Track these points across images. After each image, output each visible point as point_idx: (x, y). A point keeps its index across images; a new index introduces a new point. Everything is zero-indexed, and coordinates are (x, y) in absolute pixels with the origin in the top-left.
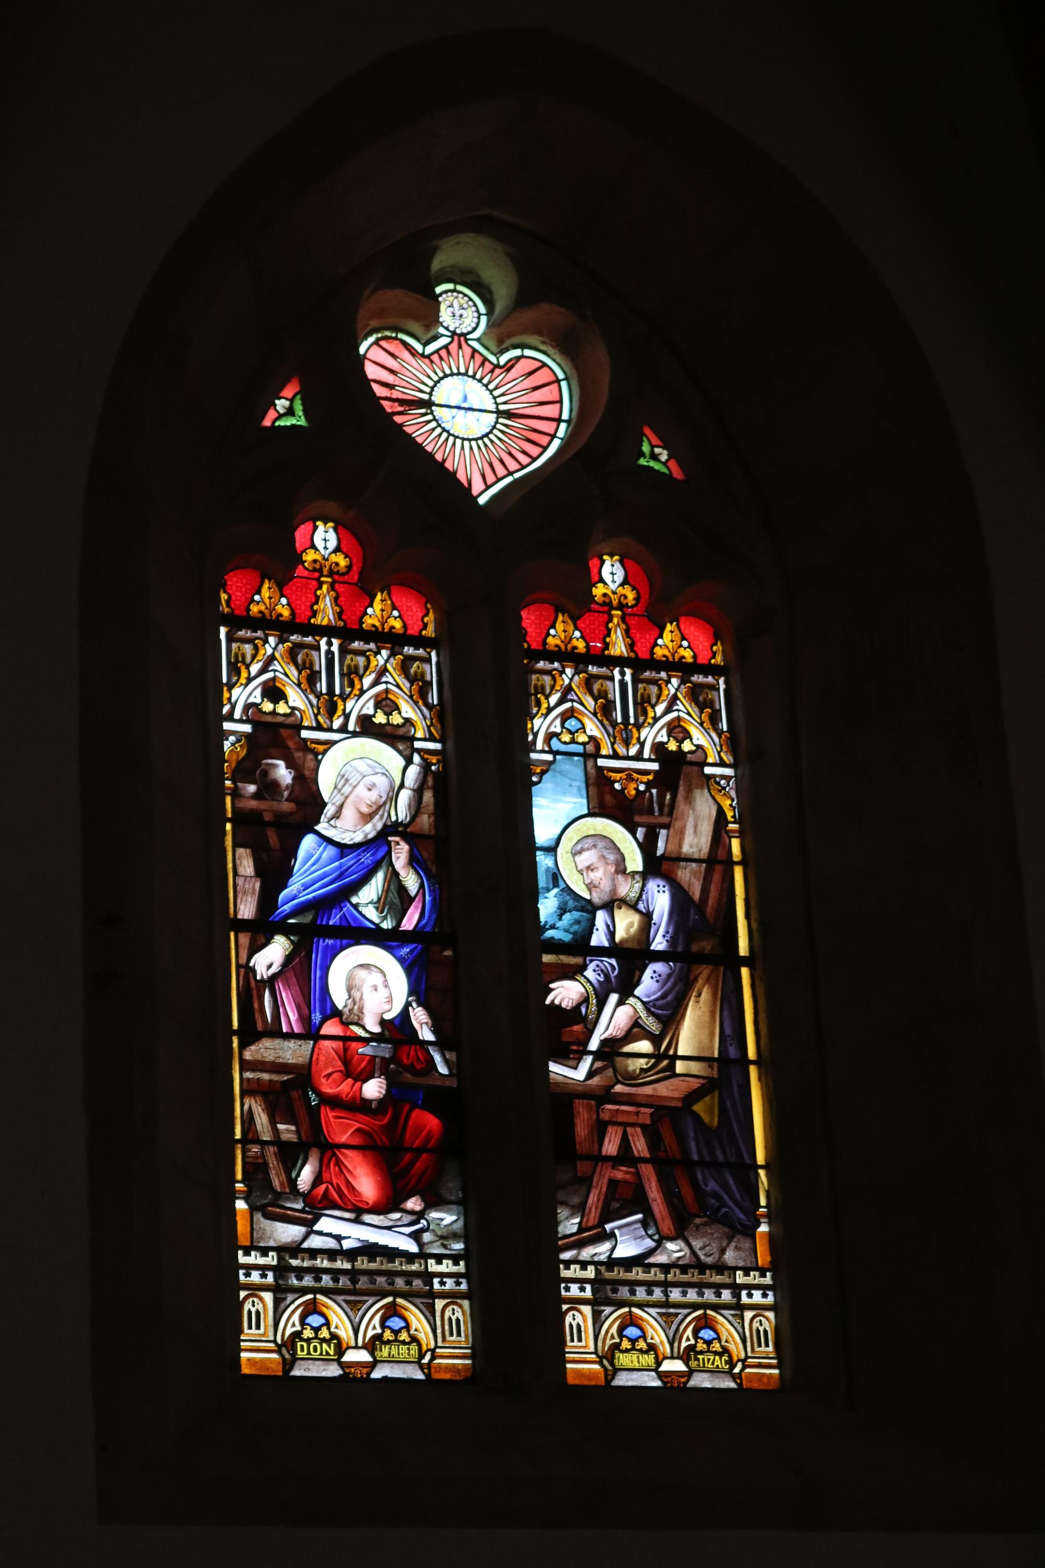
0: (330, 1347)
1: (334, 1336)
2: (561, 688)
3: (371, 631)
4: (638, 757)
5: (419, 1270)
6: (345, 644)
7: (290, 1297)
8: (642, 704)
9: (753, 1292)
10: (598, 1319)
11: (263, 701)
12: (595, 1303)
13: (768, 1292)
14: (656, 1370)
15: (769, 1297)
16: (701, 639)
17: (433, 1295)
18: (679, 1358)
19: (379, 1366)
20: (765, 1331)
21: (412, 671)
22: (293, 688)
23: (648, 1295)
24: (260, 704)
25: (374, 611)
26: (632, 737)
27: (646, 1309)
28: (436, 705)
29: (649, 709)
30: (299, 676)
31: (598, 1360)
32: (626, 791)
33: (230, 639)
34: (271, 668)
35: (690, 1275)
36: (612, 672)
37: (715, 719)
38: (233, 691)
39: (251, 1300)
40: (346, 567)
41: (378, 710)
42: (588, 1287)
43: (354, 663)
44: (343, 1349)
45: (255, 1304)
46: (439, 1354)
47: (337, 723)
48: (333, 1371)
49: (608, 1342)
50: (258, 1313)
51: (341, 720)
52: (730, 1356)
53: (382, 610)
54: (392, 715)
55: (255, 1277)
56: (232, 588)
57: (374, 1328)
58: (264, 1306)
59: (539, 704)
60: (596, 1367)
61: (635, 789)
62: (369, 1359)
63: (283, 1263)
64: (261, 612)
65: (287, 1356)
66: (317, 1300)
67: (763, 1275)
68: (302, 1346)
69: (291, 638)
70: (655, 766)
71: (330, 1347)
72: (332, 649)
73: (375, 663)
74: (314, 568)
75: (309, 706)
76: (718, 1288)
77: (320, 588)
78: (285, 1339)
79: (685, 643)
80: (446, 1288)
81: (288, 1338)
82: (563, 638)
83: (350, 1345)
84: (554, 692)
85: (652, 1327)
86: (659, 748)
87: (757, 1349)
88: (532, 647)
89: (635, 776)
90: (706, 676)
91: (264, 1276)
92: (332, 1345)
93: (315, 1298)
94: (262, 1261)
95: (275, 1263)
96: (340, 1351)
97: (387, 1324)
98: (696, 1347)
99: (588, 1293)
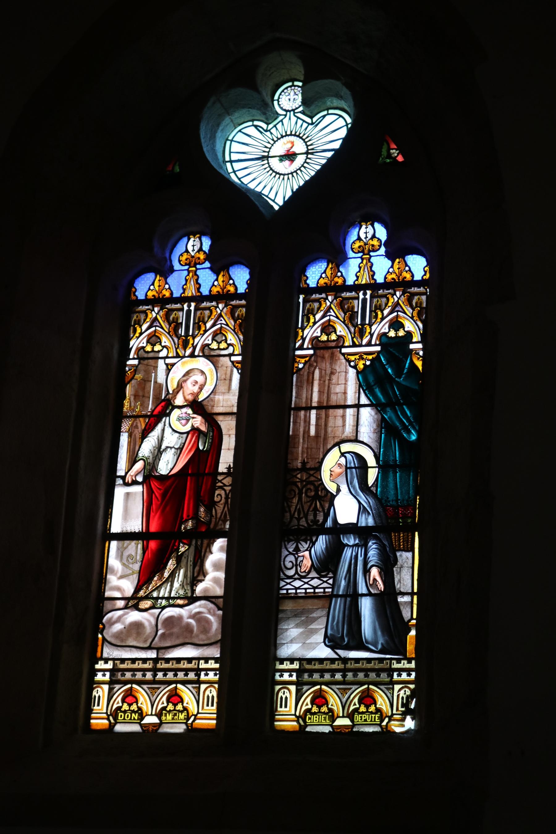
2: (150, 319)
3: (392, 282)
4: (369, 344)
5: (386, 667)
6: (198, 305)
7: (305, 688)
8: (198, 323)
9: (208, 672)
10: (299, 695)
11: (147, 345)
12: (299, 684)
13: (292, 673)
14: (140, 723)
15: (279, 677)
16: (314, 270)
17: (199, 682)
18: (155, 715)
19: (164, 725)
20: (213, 697)
21: (236, 315)
24: (320, 337)
25: (218, 283)
26: (366, 332)
27: (380, 686)
29: (311, 317)
30: (235, 324)
31: (296, 719)
32: (358, 366)
33: (305, 301)
34: (328, 314)
35: (148, 664)
36: (183, 306)
38: (372, 327)
39: (282, 691)
41: (148, 344)
42: (295, 674)
43: (138, 318)
45: (285, 693)
46: (277, 719)
47: (188, 352)
48: (136, 728)
50: (286, 698)
51: (191, 350)
52: (188, 713)
53: (159, 286)
54: (330, 335)
55: (286, 677)
56: (320, 271)
59: (135, 331)
60: (295, 723)
61: (363, 364)
62: (158, 721)
63: (302, 667)
64: (393, 279)
65: (112, 721)
68: (121, 716)
70: (311, 352)
72: (363, 297)
74: (359, 251)
78: (350, 712)
79: (152, 287)
80: (411, 678)
81: (351, 712)
82: (222, 286)
83: (147, 714)
84: (319, 312)
85: (143, 695)
86: (315, 340)
87: (205, 707)
88: (138, 299)
89: (365, 357)
90: (419, 287)
91: (409, 675)
93: (368, 687)
94: (407, 666)
95: (298, 667)
96: (142, 717)
97: (170, 700)
98: (359, 709)
99: (294, 678)
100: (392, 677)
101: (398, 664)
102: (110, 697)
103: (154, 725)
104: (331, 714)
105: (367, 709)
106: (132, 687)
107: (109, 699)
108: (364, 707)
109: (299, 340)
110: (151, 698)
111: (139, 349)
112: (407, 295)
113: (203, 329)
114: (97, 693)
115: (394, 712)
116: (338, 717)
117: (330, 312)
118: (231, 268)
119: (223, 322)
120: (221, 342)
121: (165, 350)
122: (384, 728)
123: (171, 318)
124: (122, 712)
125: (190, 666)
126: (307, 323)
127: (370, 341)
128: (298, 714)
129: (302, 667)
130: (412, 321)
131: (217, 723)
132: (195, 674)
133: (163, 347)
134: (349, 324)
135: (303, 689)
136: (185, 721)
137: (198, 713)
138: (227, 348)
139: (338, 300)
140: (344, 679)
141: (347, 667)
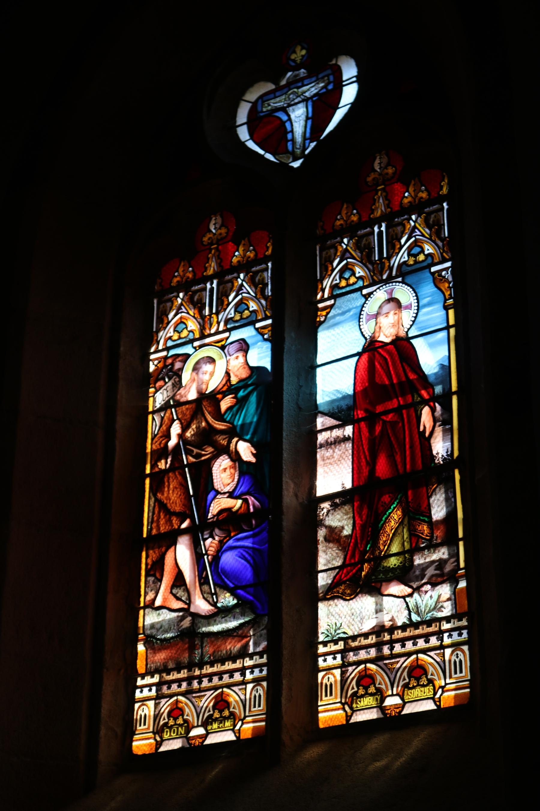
0: (182, 730)
1: (186, 721)
9: (452, 633)
19: (407, 705)
20: (260, 696)
22: (429, 243)
23: (426, 643)
27: (429, 653)
28: (270, 296)
30: (256, 291)
34: (414, 234)
37: (439, 233)
40: (226, 233)
44: (190, 729)
49: (206, 715)
50: (461, 661)
57: (209, 711)
58: (149, 711)
66: (224, 693)
67: (262, 657)
69: (426, 210)
71: (182, 730)
72: (382, 229)
73: (409, 226)
75: (261, 307)
76: (426, 637)
77: (377, 194)
84: (336, 257)
92: (184, 728)
95: (342, 647)
100: (442, 640)
101: (428, 628)
102: (343, 682)
103: (396, 706)
104: (186, 725)
105: (418, 682)
106: (222, 691)
107: (343, 683)
108: (218, 712)
109: (387, 270)
110: (390, 675)
111: (400, 266)
112: (251, 275)
113: (330, 268)
114: (143, 711)
115: (247, 714)
116: (194, 727)
117: (182, 309)
118: (399, 183)
119: (245, 291)
120: (349, 278)
121: (191, 334)
122: (438, 702)
123: (431, 222)
124: (168, 727)
125: (430, 630)
126: (392, 251)
127: (323, 296)
128: (343, 701)
129: (347, 646)
130: (257, 301)
131: (266, 725)
132: (437, 638)
133: (190, 331)
134: (437, 239)
135: (348, 670)
136: (232, 728)
137: (446, 684)
138: (356, 282)
139: (422, 217)
140: (391, 652)
141: (393, 638)
